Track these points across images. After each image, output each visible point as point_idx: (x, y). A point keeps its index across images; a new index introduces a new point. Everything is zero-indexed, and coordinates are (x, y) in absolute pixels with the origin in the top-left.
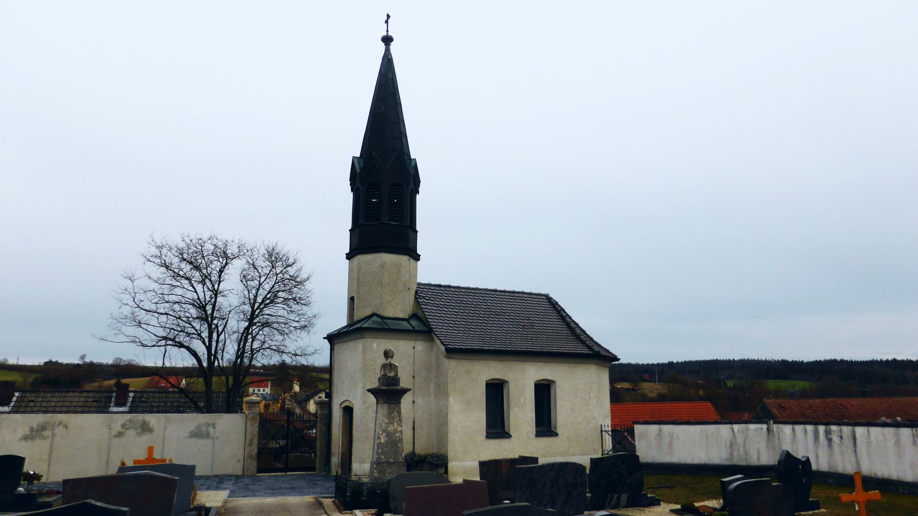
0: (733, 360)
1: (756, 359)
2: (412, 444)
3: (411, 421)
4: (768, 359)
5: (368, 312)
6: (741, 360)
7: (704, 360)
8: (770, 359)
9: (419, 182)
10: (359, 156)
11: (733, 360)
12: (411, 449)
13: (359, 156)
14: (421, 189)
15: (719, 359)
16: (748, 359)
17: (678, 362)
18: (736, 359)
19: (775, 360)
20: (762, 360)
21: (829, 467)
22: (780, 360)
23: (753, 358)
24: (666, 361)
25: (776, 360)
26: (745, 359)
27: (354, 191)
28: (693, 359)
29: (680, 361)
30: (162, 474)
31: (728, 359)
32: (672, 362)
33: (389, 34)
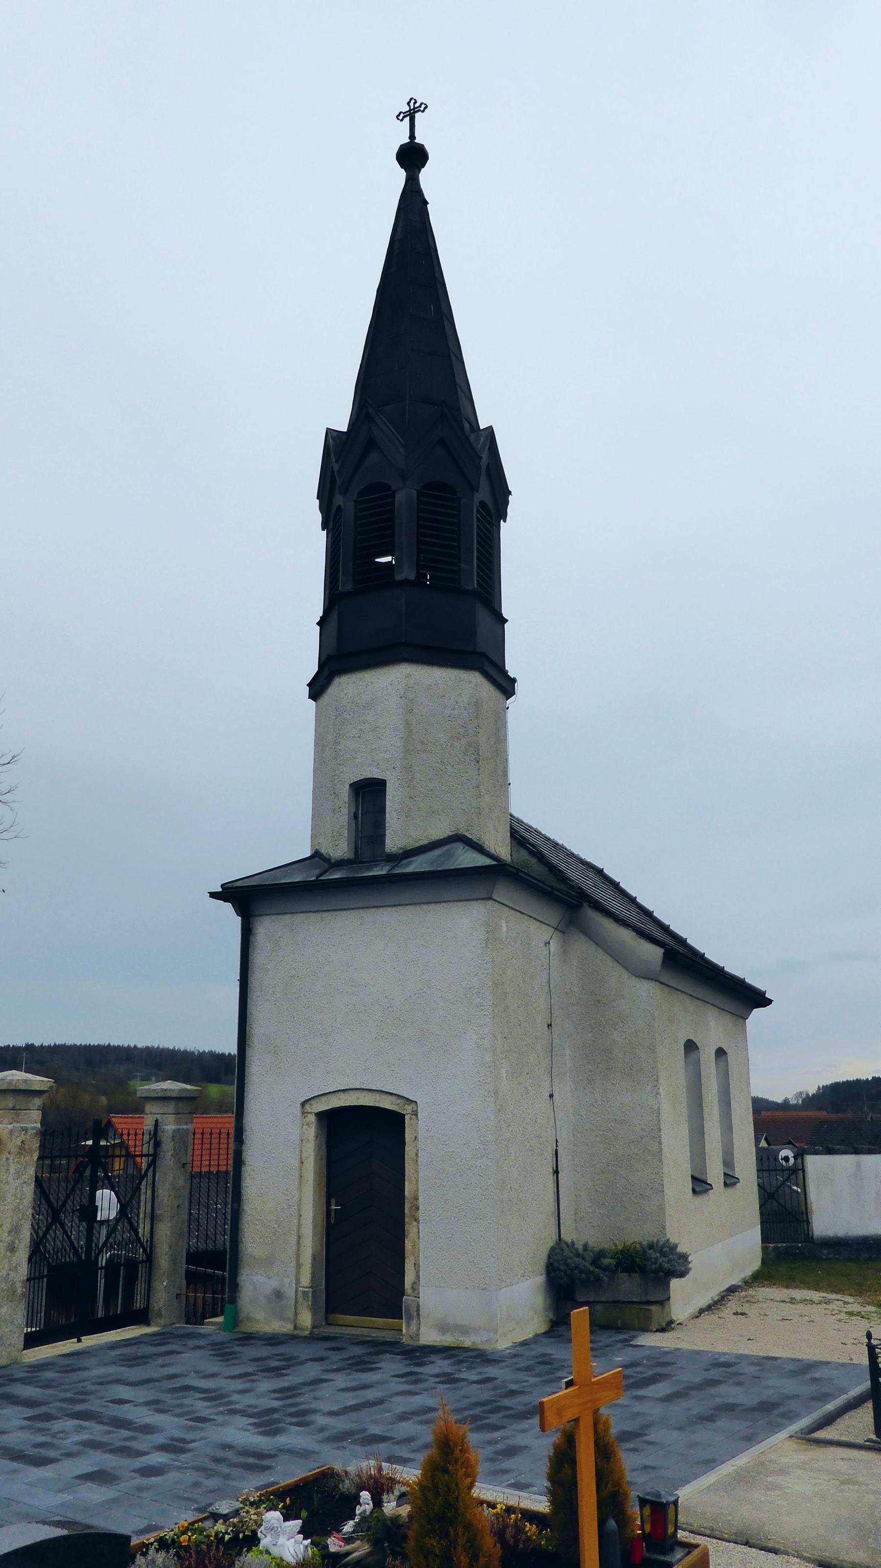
0: (135, 1046)
1: (171, 1048)
2: (553, 1220)
3: (550, 1149)
4: (188, 1050)
5: (439, 830)
6: (147, 1048)
7: (132, 1045)
8: (193, 1049)
9: (506, 492)
10: (346, 430)
11: (135, 1046)
12: (555, 1237)
13: (346, 430)
14: (512, 509)
15: (92, 1044)
16: (158, 1047)
17: (109, 1044)
18: (139, 1046)
19: (199, 1051)
20: (179, 1050)
21: (541, 1274)
22: (207, 1051)
23: (166, 1046)
24: (21, 1043)
25: (201, 1051)
26: (153, 1047)
27: (331, 526)
28: (70, 1042)
29: (46, 1044)
30: (121, 1283)
31: (126, 1045)
32: (32, 1045)
33: (418, 140)
